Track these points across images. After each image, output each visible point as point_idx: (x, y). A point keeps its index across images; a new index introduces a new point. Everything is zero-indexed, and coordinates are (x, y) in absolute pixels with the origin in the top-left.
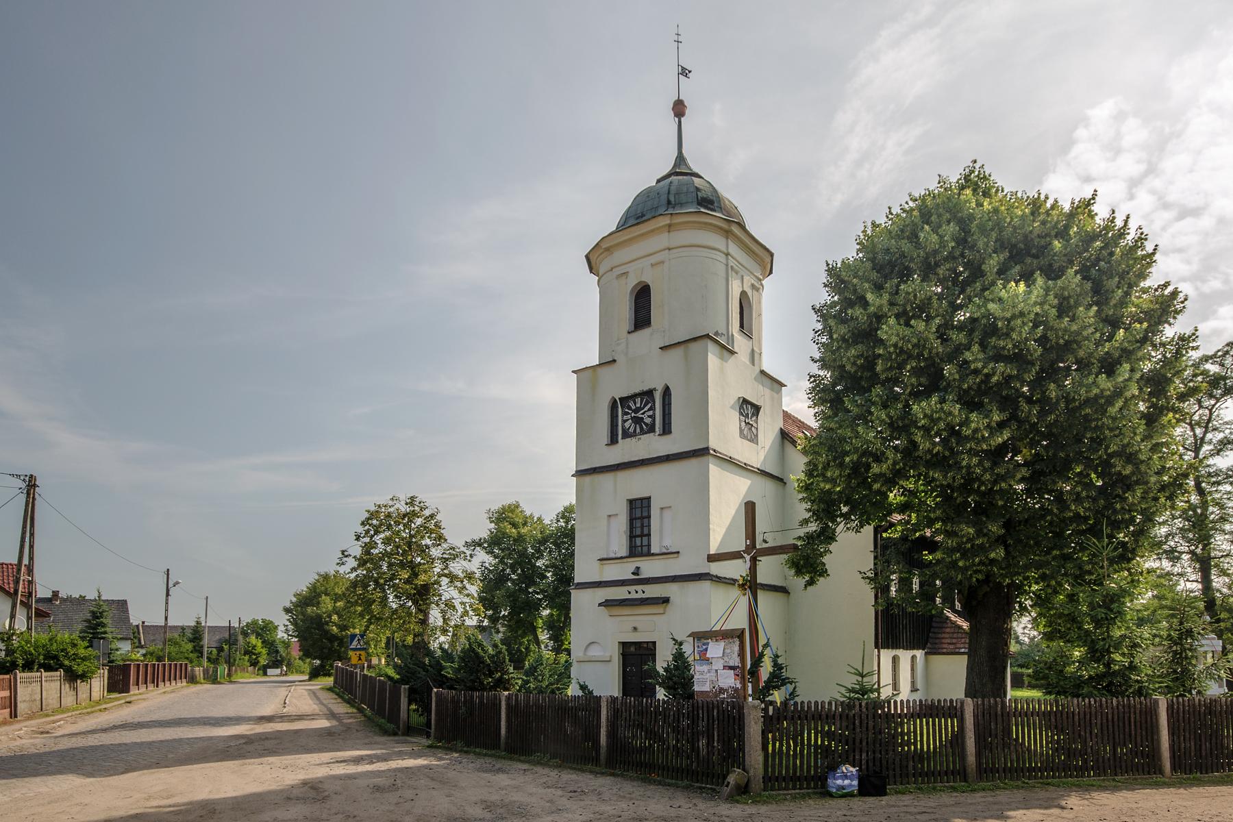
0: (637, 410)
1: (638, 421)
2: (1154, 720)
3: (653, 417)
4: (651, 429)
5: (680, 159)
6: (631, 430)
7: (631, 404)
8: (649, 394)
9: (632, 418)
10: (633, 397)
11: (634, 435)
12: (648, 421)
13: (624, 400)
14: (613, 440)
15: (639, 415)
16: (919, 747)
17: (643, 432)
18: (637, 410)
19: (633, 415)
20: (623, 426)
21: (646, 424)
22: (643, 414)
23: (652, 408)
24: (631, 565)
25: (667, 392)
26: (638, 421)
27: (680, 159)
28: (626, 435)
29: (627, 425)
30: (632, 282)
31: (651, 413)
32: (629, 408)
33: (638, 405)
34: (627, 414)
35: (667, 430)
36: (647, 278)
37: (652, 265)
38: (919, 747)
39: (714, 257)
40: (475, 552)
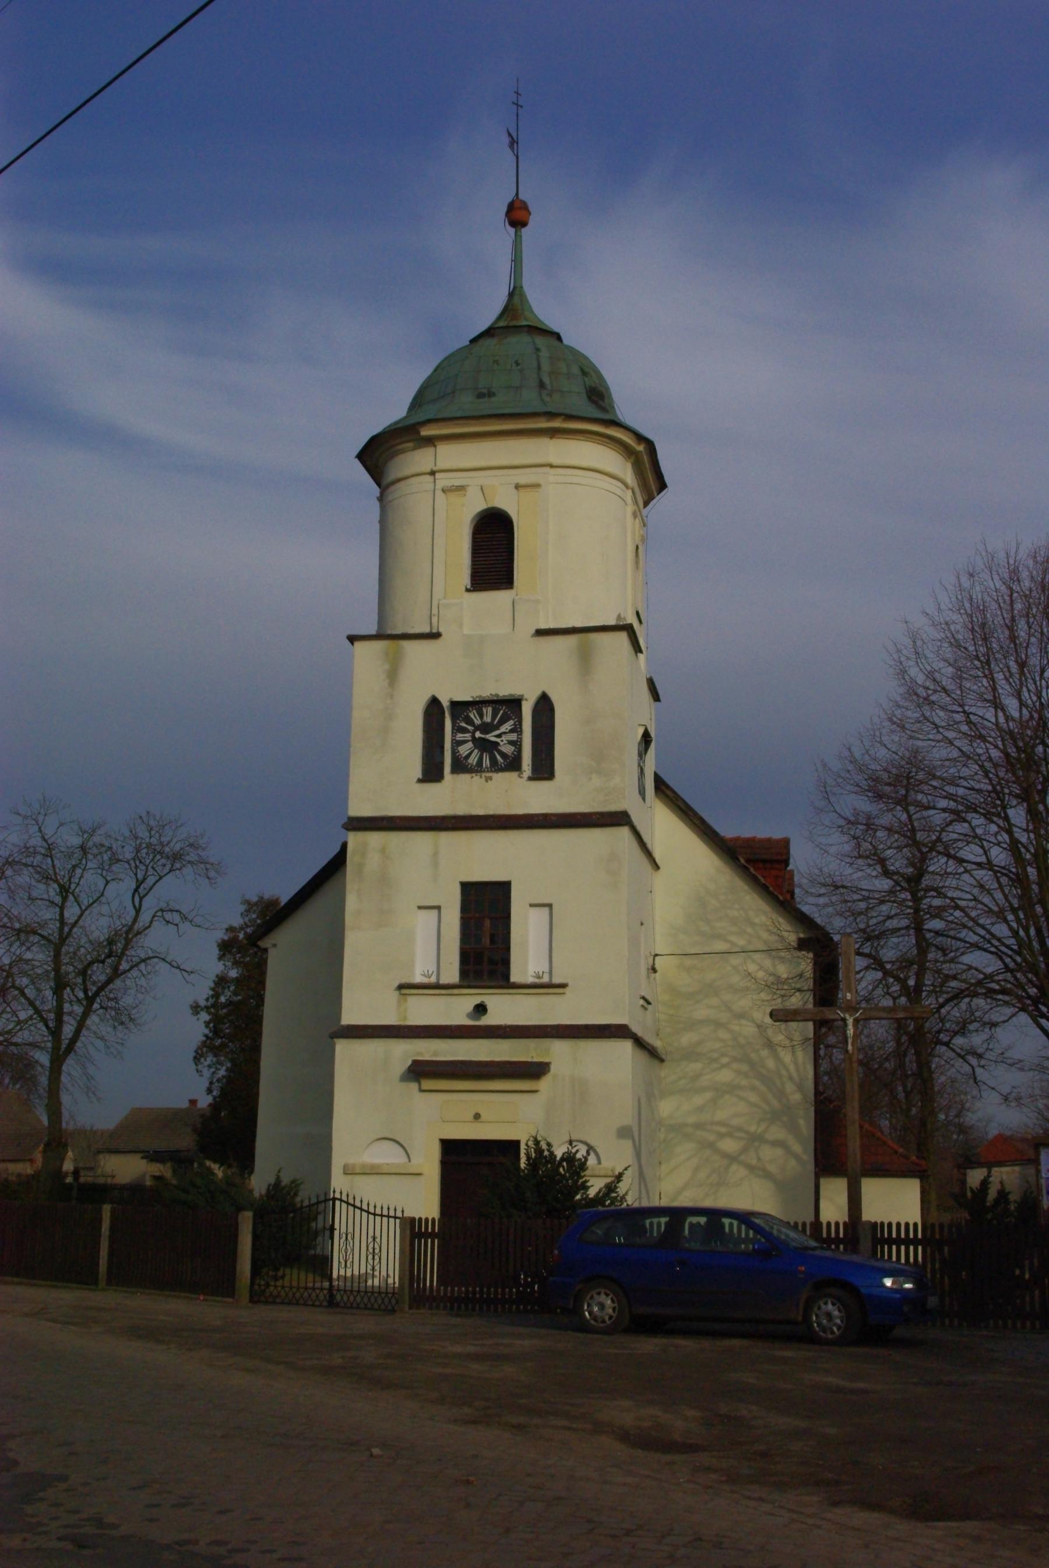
0: (486, 728)
1: (486, 747)
2: (1008, 1163)
3: (517, 744)
4: (513, 764)
5: (515, 293)
6: (473, 760)
7: (473, 715)
8: (513, 704)
9: (474, 740)
10: (478, 704)
11: (478, 769)
12: (508, 749)
13: (459, 708)
14: (432, 773)
15: (491, 737)
16: (428, 1284)
17: (495, 767)
18: (486, 728)
19: (478, 734)
20: (454, 752)
21: (504, 755)
22: (499, 736)
23: (517, 729)
24: (466, 1002)
25: (545, 706)
26: (486, 747)
27: (515, 293)
28: (460, 766)
29: (464, 750)
30: (474, 505)
31: (513, 737)
32: (470, 722)
33: (488, 719)
34: (464, 730)
35: (544, 769)
36: (506, 502)
37: (517, 487)
38: (428, 1284)
39: (575, 480)
40: (985, 1046)
